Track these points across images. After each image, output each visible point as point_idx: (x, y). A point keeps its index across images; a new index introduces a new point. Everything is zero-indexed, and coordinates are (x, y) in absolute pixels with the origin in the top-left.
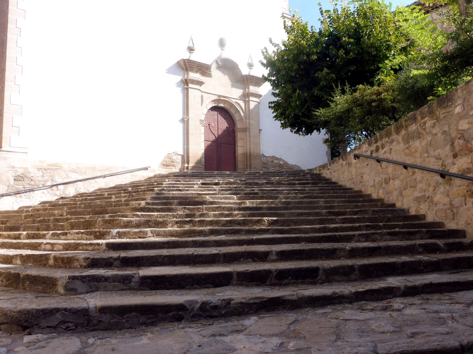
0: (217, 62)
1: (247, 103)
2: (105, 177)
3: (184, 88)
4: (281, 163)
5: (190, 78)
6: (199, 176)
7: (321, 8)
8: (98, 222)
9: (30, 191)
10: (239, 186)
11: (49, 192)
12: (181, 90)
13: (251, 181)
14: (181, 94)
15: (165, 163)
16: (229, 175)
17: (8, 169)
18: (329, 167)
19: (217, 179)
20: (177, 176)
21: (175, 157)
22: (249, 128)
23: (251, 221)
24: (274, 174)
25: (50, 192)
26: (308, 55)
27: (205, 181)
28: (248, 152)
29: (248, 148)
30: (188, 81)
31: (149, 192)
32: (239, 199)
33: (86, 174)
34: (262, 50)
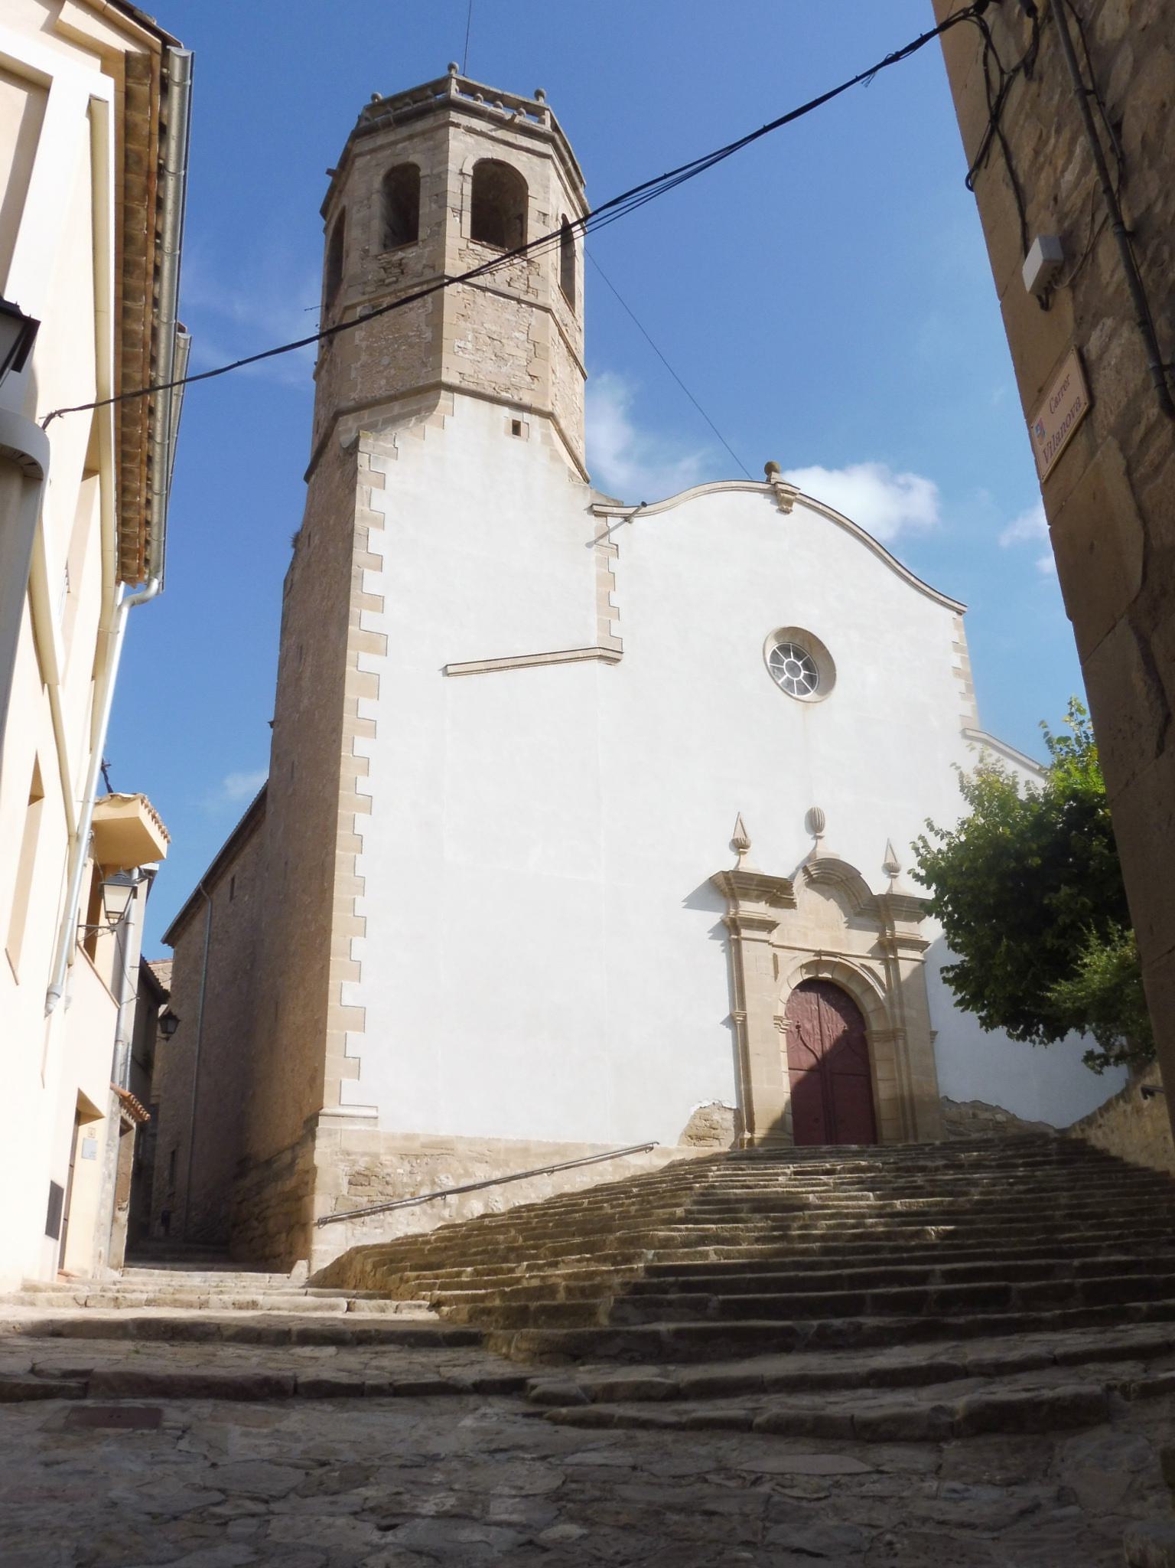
0: (806, 870)
1: (892, 965)
2: (552, 1172)
3: (730, 941)
4: (1000, 1117)
5: (742, 914)
6: (786, 1158)
7: (1046, 734)
8: (608, 1242)
9: (383, 1210)
10: (883, 1174)
11: (425, 1213)
12: (722, 945)
13: (909, 1164)
14: (724, 954)
15: (693, 1132)
16: (858, 1152)
17: (335, 1158)
18: (1101, 1121)
19: (830, 1162)
20: (734, 1159)
21: (716, 1117)
22: (905, 1032)
23: (902, 1235)
24: (969, 1146)
25: (429, 1211)
26: (1020, 857)
27: (801, 1167)
28: (906, 1093)
29: (905, 1082)
30: (738, 922)
31: (684, 1192)
32: (878, 1198)
33: (508, 1166)
34: (914, 843)
